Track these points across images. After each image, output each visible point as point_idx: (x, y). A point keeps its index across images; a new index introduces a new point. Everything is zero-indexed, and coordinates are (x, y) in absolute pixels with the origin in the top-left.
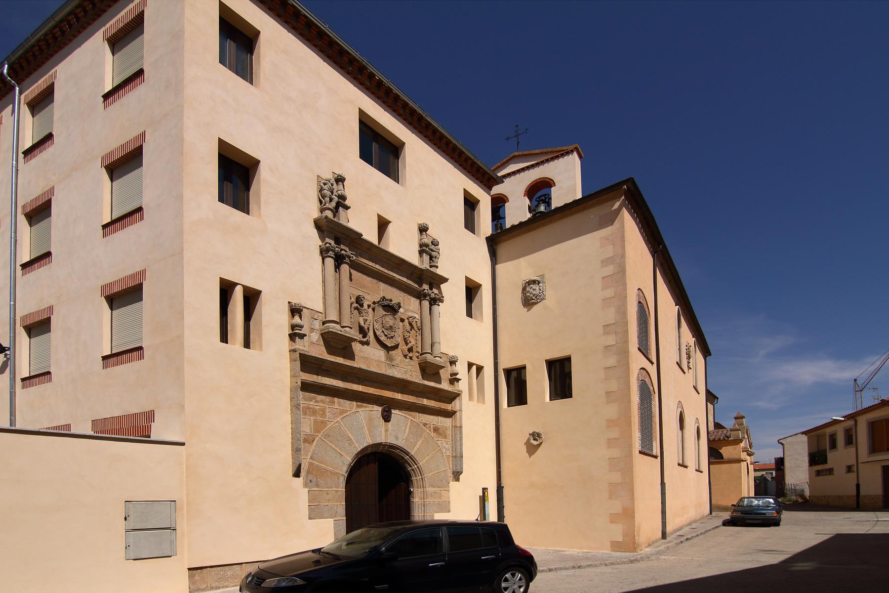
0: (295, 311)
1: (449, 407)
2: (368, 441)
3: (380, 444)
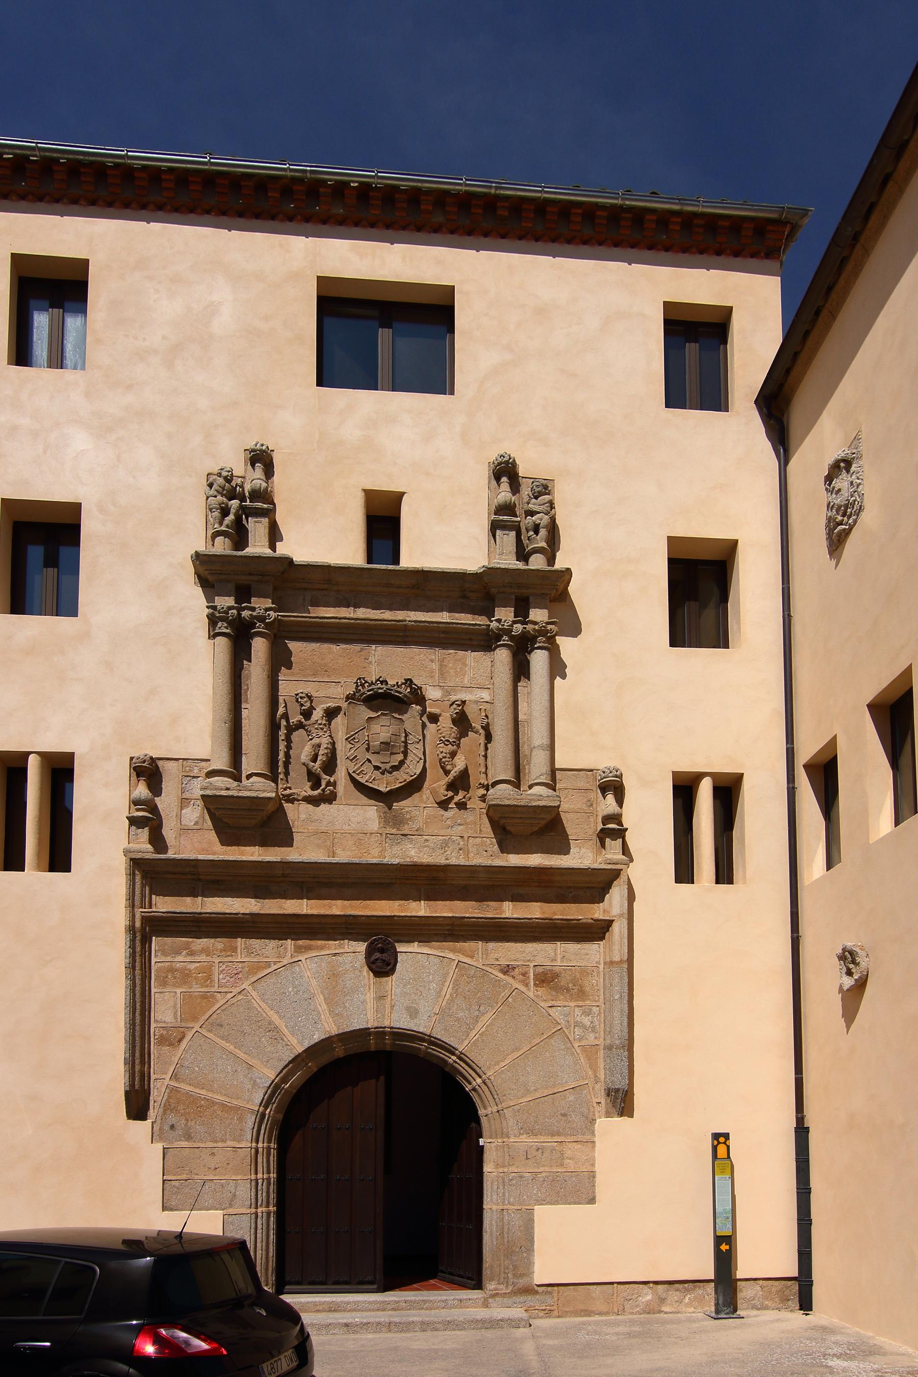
0: (148, 772)
1: (597, 912)
2: (327, 1026)
3: (364, 1033)
